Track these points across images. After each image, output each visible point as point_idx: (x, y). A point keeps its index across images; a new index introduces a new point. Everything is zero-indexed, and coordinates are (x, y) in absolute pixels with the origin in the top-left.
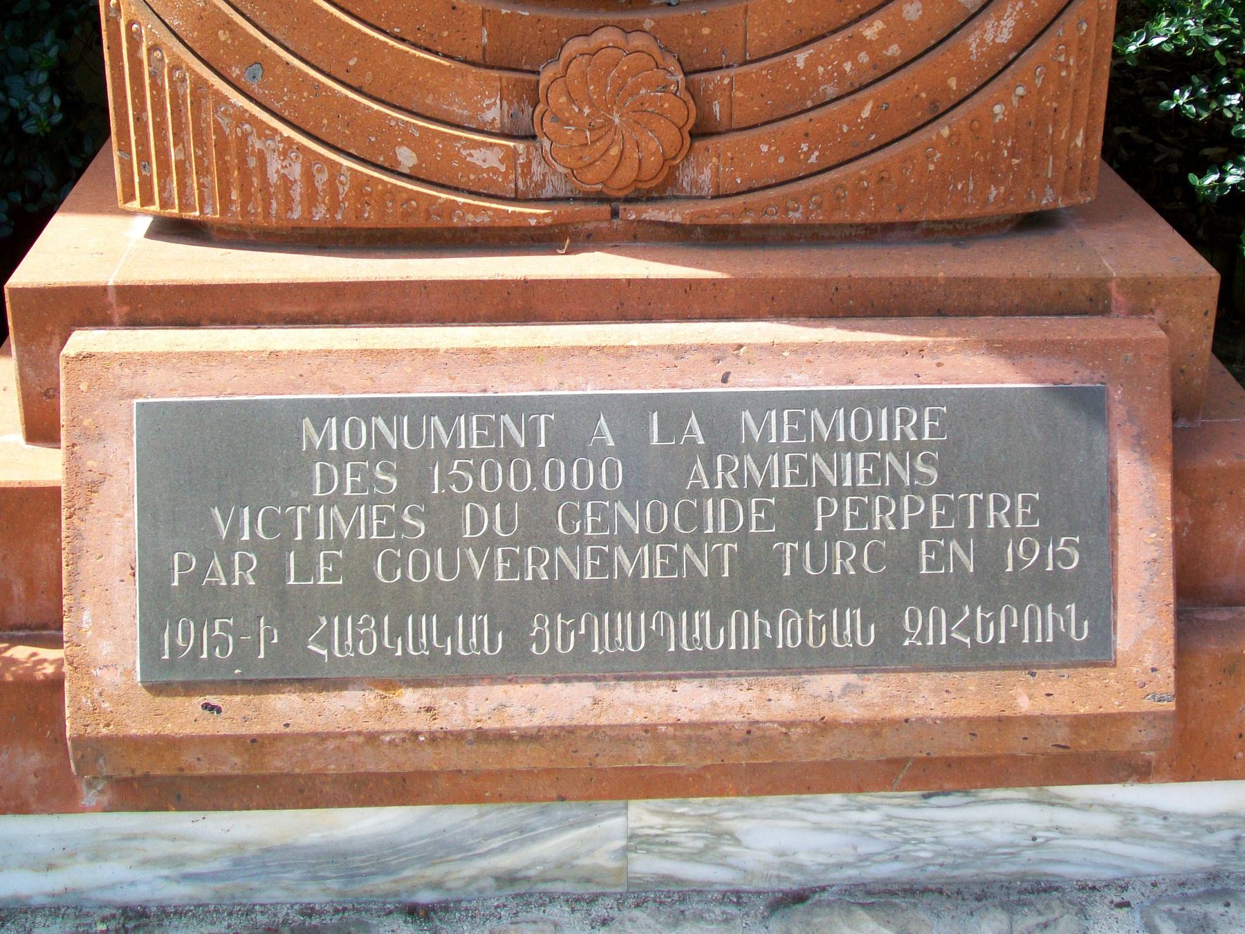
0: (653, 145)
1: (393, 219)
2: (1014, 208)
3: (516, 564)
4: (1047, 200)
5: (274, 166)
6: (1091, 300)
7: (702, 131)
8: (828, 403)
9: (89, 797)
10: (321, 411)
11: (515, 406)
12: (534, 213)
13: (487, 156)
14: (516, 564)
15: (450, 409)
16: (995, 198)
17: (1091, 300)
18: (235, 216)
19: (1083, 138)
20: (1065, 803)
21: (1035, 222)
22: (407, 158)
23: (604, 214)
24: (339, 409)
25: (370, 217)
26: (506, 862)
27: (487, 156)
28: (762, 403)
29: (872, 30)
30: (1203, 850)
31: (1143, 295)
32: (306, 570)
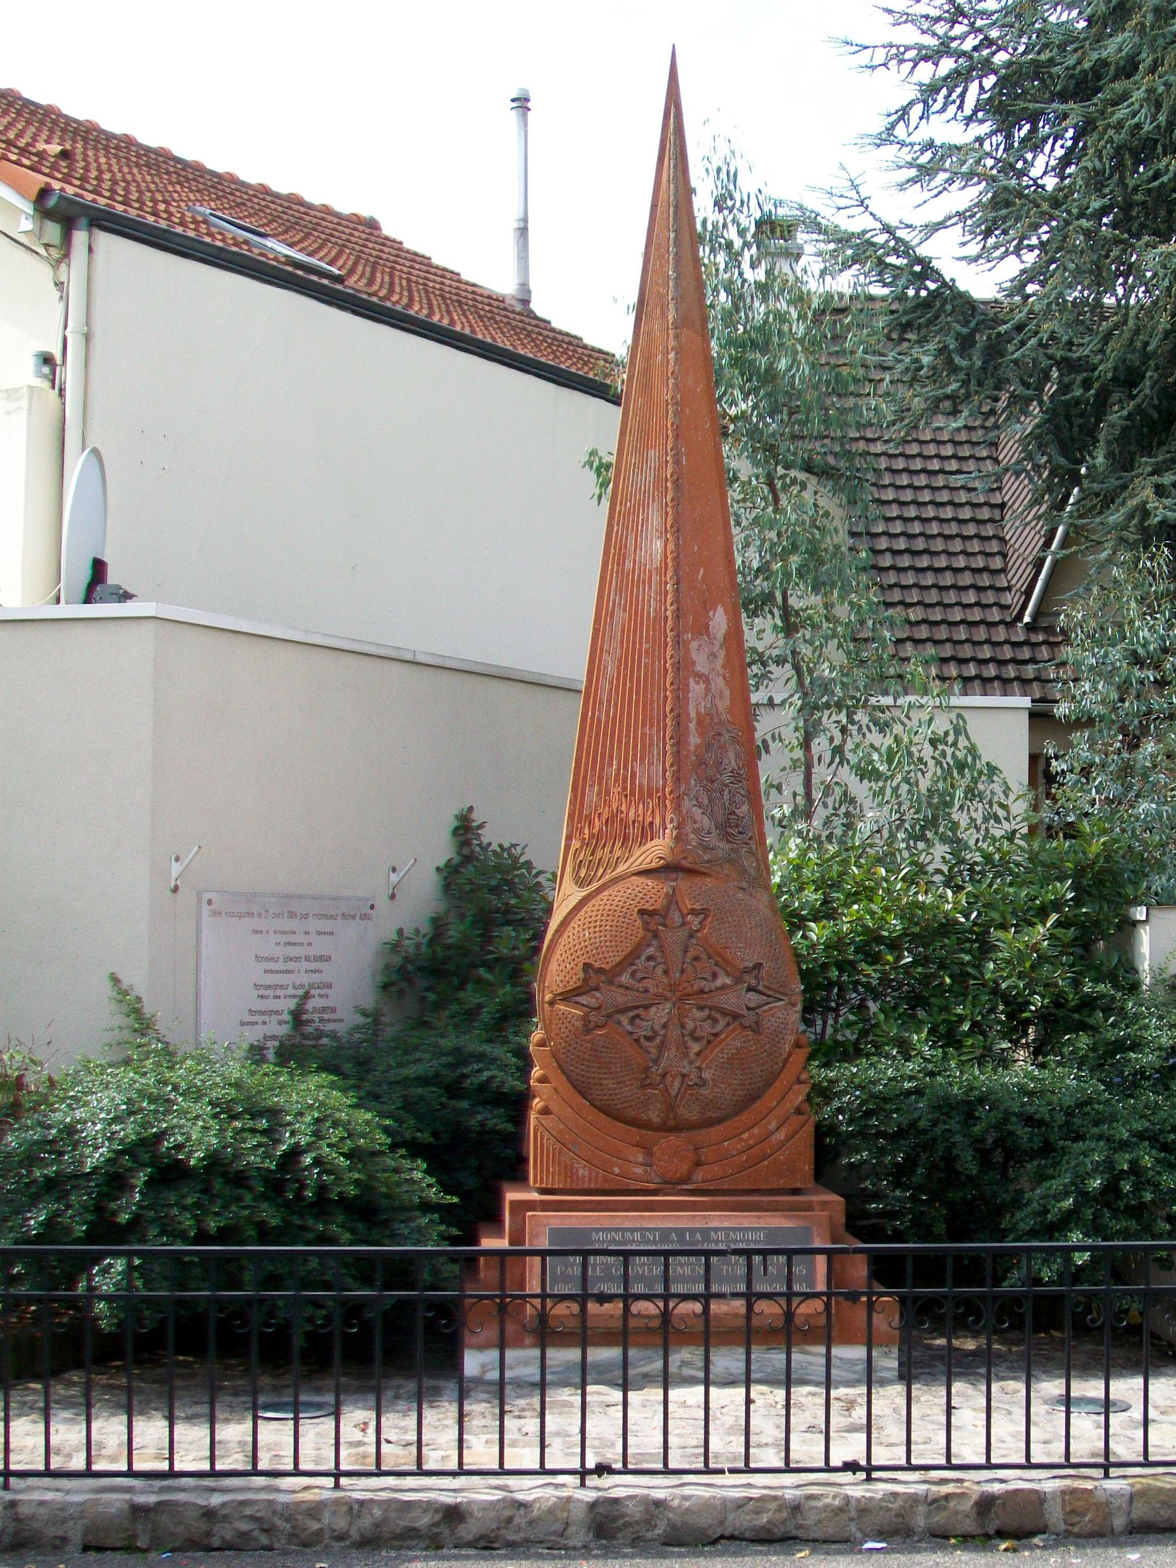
0: (684, 1168)
1: (613, 1186)
2: (788, 1186)
3: (651, 1270)
4: (798, 1185)
5: (581, 1172)
6: (809, 1207)
7: (698, 1164)
8: (734, 1230)
9: (528, 1342)
10: (597, 1230)
11: (650, 1230)
12: (652, 1186)
13: (639, 1170)
14: (651, 1270)
15: (632, 1230)
16: (781, 1183)
17: (809, 1207)
18: (568, 1186)
19: (808, 1167)
20: (811, 1354)
21: (796, 1192)
22: (617, 1170)
23: (671, 1184)
24: (603, 1230)
25: (606, 1186)
26: (645, 1369)
27: (639, 1170)
28: (716, 1230)
29: (745, 1136)
30: (855, 1372)
31: (824, 1205)
32: (594, 1270)
